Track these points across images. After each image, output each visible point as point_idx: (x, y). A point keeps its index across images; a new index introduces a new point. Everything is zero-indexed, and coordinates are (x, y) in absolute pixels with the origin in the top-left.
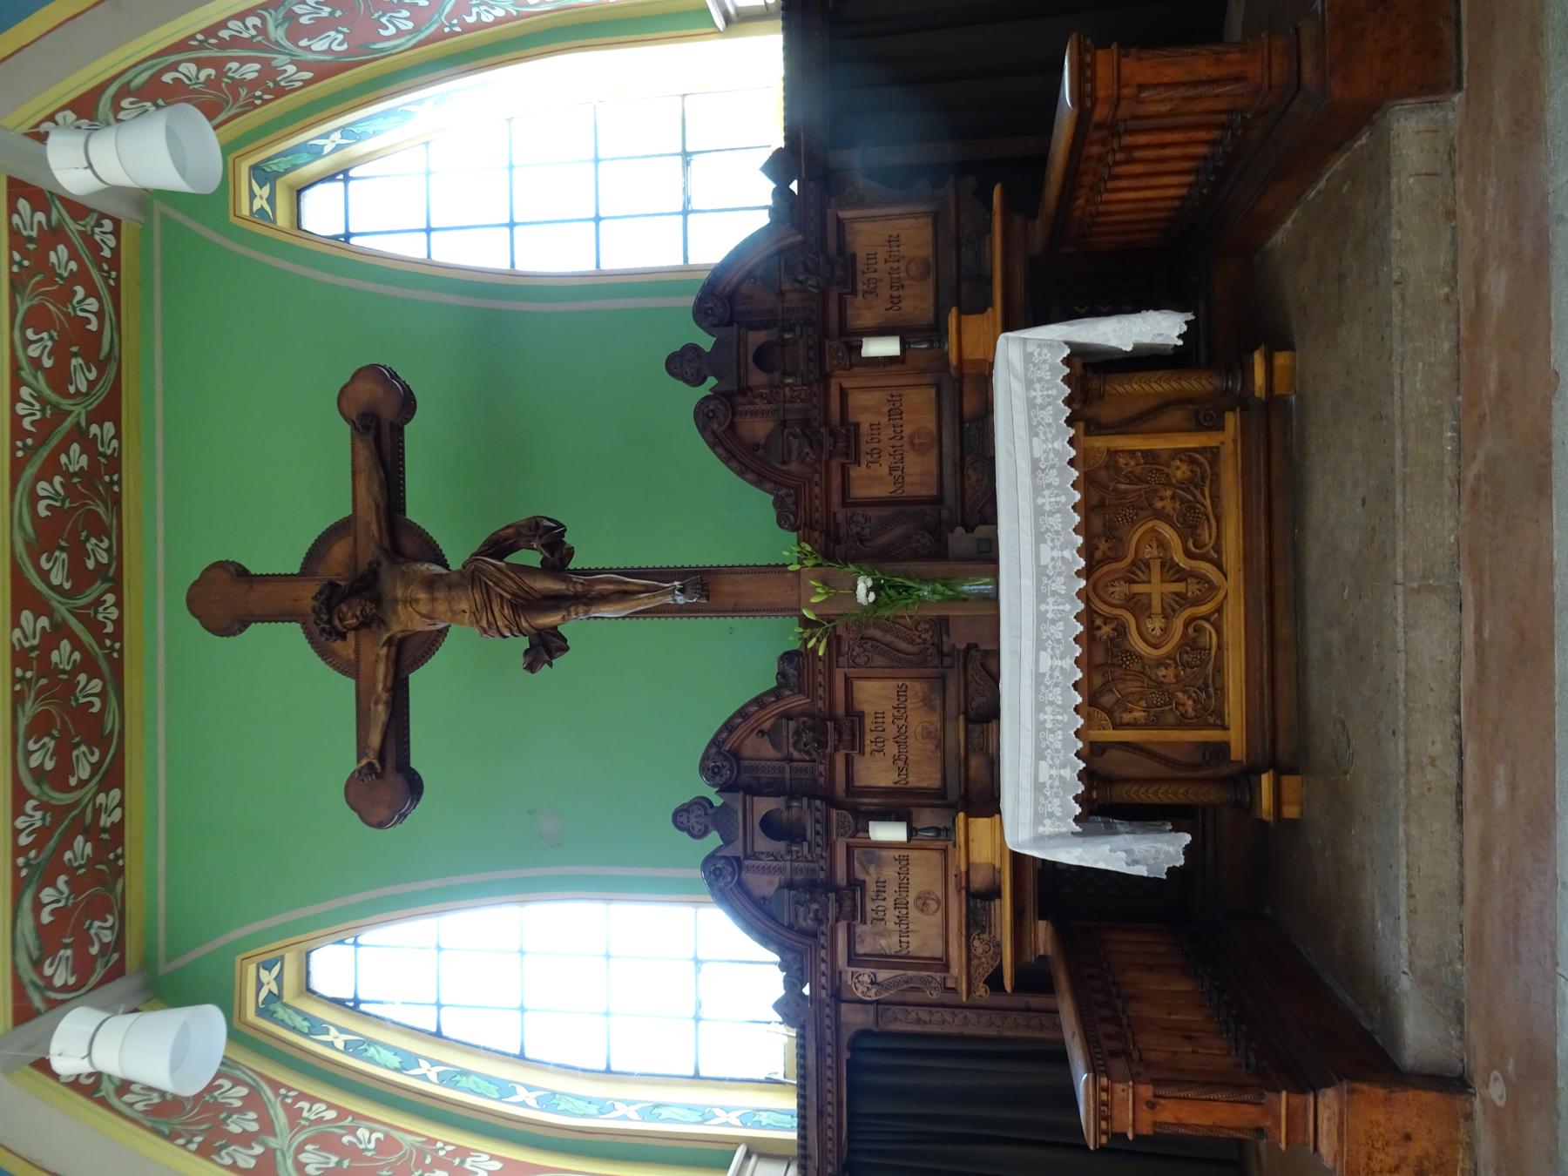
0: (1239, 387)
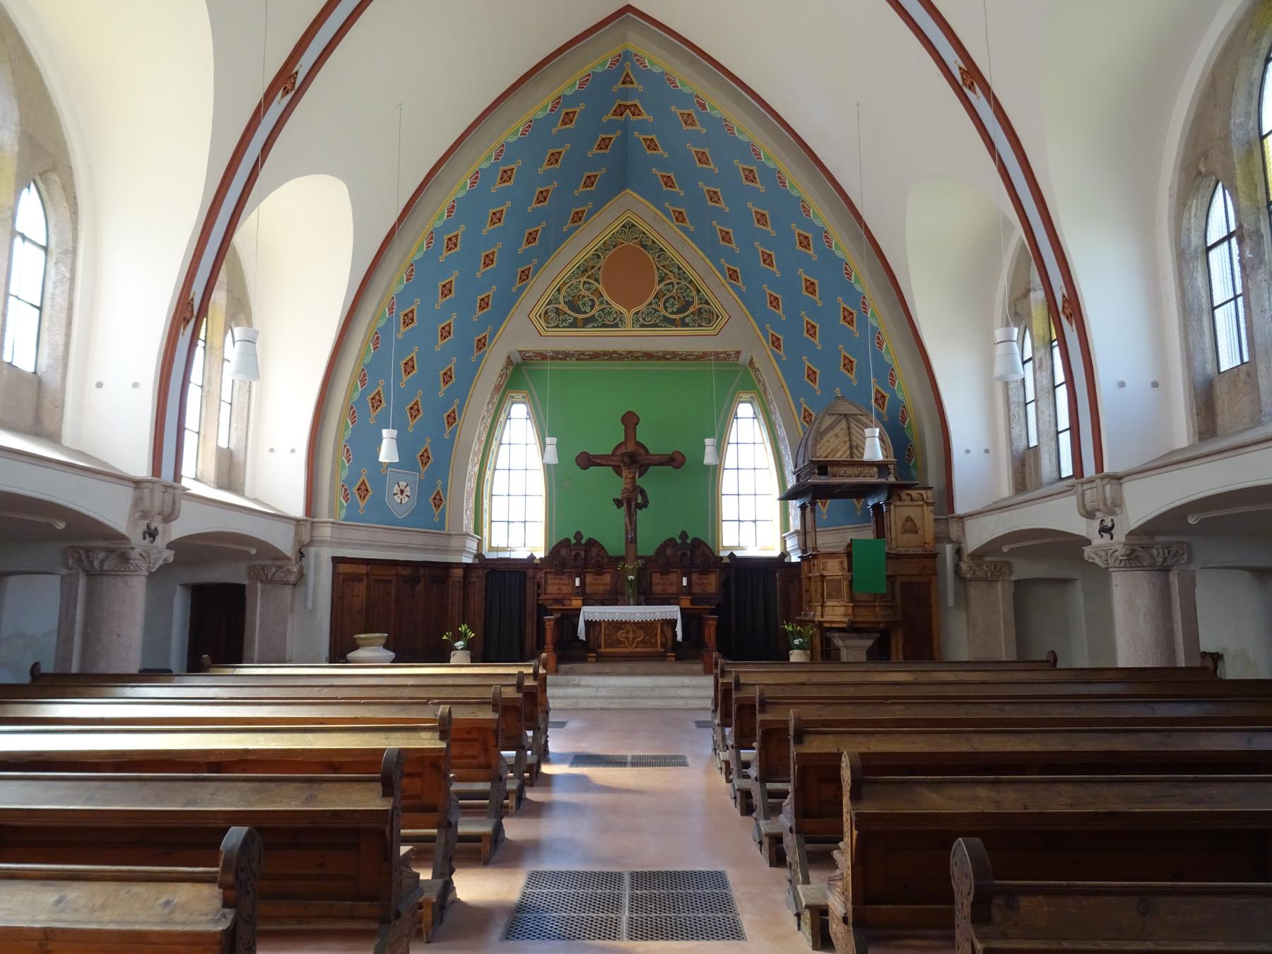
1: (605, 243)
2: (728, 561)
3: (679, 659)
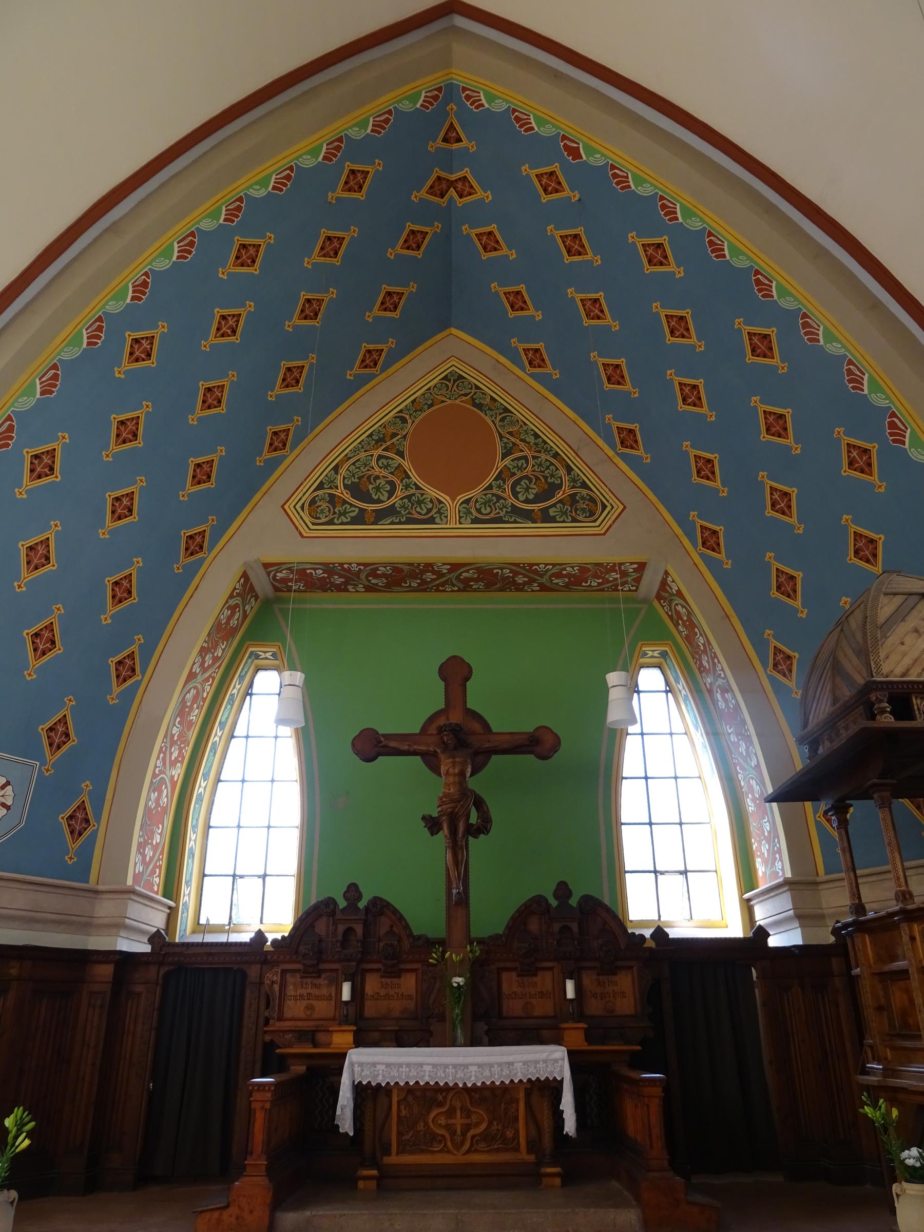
0: (546, 1161)
1: (413, 401)
2: (651, 944)
3: (569, 1179)
